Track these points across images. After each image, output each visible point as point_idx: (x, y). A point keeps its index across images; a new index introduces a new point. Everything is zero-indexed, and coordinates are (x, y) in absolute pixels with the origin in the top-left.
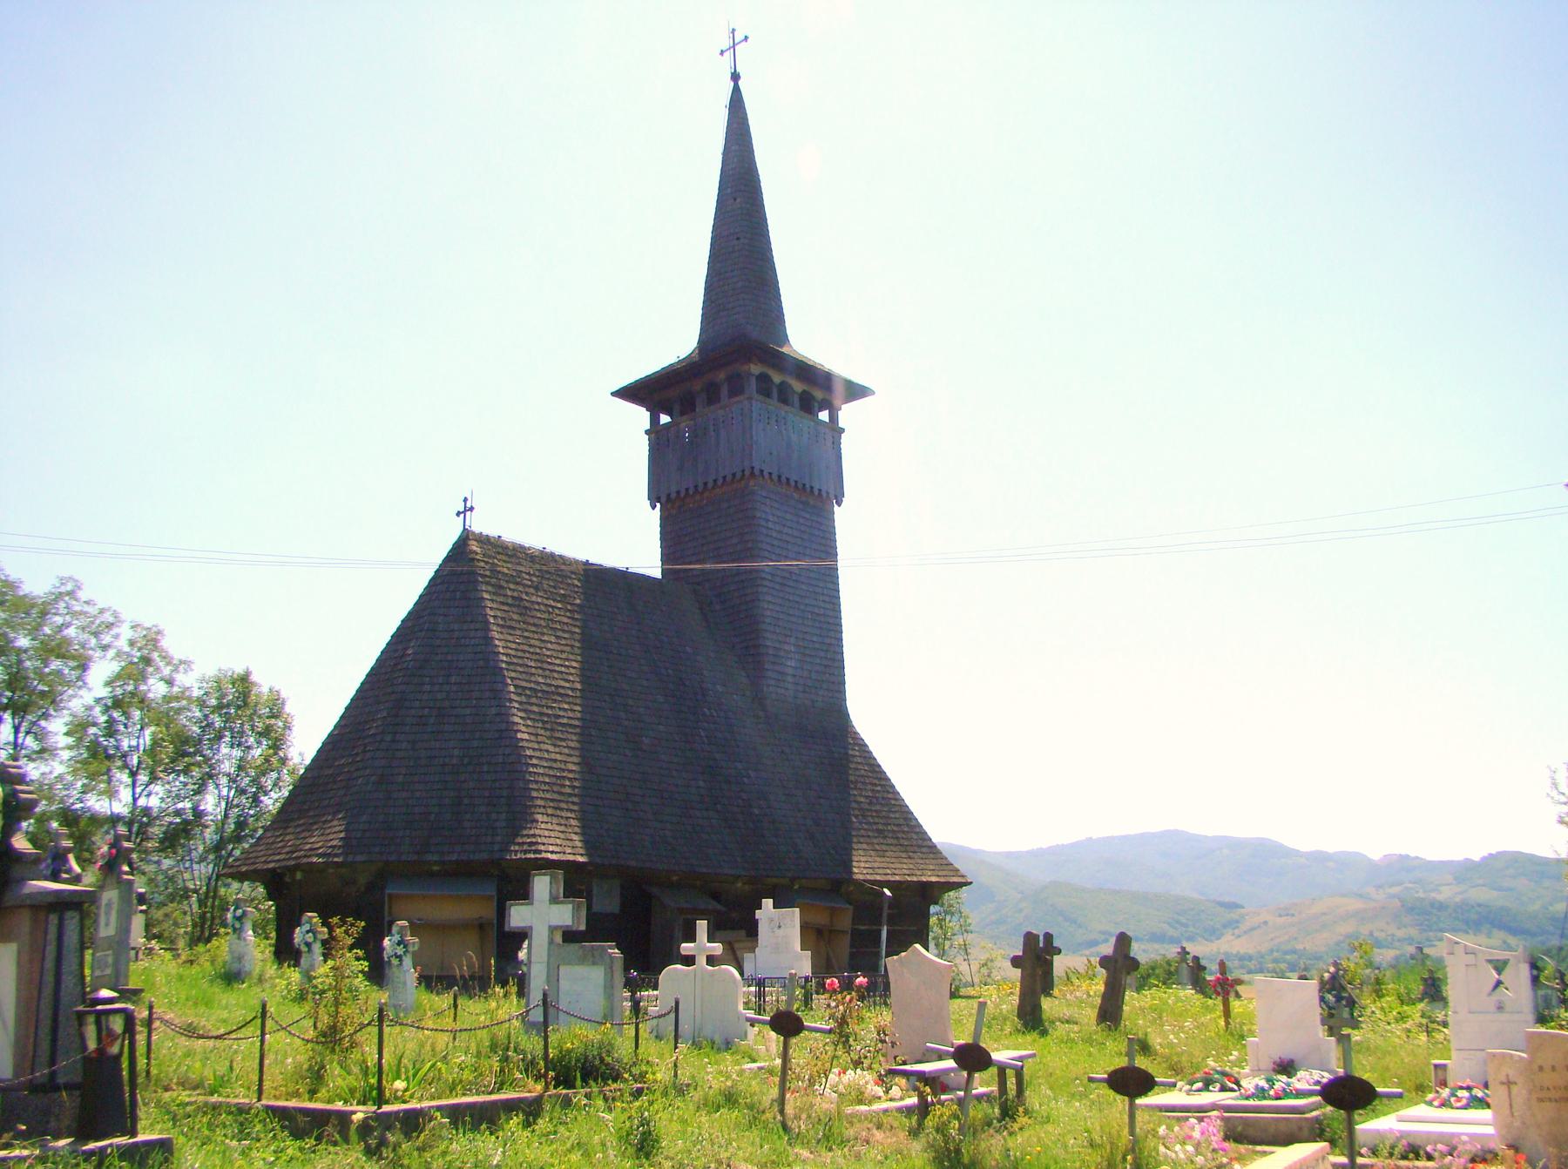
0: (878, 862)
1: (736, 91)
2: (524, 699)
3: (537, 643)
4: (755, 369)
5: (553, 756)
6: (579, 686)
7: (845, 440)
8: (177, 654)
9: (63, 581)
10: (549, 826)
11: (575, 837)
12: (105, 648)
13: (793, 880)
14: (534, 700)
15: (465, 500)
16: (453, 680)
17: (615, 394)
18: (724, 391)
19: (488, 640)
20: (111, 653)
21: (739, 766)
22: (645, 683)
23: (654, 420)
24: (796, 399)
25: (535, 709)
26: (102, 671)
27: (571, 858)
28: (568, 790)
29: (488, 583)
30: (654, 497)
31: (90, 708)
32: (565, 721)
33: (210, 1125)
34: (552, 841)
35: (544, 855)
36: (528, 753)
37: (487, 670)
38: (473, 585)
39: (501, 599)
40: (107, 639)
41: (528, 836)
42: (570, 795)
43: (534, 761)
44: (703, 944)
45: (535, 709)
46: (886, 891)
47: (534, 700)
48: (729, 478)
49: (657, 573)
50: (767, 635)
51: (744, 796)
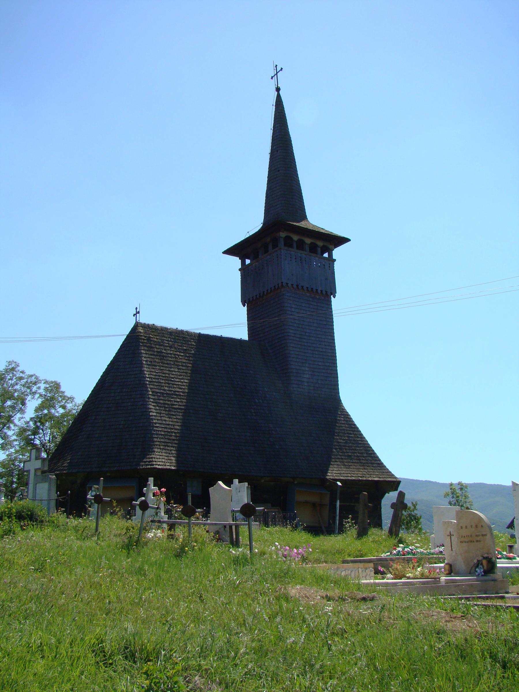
0: (344, 470)
2: (156, 397)
3: (167, 372)
4: (283, 235)
5: (167, 423)
6: (186, 391)
8: (68, 394)
9: (10, 363)
10: (160, 454)
11: (173, 458)
12: (35, 393)
14: (162, 398)
15: (136, 308)
16: (124, 390)
17: (224, 253)
18: (270, 246)
19: (142, 372)
20: (37, 396)
23: (243, 263)
24: (307, 248)
25: (162, 402)
26: (32, 405)
27: (168, 467)
28: (173, 438)
29: (145, 346)
30: (244, 303)
31: (28, 422)
32: (177, 407)
33: (92, 612)
34: (160, 460)
35: (155, 466)
36: (154, 421)
37: (140, 385)
38: (143, 346)
39: (151, 353)
40: (34, 389)
41: (149, 458)
42: (174, 440)
43: (157, 425)
44: (353, 532)
45: (162, 402)
46: (339, 483)
47: (162, 398)
48: (273, 289)
51: (271, 439)
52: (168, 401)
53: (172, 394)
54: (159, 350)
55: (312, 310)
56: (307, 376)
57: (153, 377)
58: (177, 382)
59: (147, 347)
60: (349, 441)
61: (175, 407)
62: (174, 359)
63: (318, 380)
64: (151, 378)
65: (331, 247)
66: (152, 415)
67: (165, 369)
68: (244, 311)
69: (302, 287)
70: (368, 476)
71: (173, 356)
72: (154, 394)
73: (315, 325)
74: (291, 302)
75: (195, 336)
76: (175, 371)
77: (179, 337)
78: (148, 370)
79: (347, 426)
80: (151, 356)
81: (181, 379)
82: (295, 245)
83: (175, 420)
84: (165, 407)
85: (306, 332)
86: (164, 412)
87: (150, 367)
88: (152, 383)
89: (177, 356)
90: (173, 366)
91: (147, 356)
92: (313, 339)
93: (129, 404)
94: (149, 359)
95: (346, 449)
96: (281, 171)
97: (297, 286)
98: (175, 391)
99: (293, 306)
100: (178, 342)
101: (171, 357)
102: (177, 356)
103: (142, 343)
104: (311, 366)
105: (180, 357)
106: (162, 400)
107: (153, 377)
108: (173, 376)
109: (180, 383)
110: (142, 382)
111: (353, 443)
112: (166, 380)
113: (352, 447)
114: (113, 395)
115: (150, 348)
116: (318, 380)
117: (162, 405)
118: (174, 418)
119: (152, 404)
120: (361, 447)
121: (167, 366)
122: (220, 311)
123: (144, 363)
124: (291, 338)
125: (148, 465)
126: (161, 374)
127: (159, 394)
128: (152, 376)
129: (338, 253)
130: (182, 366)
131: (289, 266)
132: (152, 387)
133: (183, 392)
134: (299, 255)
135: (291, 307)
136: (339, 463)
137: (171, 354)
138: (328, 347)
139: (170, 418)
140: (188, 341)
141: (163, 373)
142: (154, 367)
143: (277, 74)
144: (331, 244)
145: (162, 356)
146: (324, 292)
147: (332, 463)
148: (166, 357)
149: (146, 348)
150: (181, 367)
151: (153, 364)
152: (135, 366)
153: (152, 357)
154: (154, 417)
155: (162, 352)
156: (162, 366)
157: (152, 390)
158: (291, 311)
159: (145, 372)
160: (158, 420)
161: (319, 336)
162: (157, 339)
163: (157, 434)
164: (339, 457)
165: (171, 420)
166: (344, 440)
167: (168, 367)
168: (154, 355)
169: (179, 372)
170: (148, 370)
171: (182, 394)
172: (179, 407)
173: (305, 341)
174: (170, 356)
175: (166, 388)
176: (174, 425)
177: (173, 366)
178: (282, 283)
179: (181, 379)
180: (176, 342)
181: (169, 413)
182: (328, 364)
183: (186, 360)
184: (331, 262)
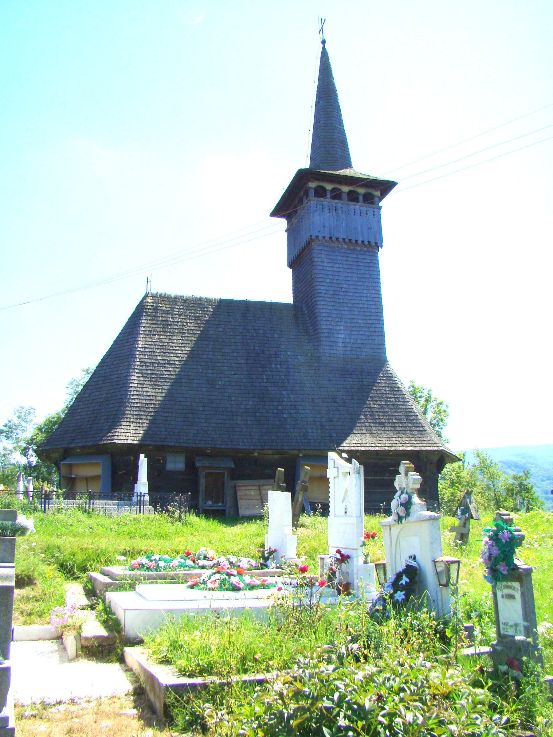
2: (144, 368)
4: (312, 185)
5: (149, 394)
10: (128, 427)
13: (299, 450)
21: (284, 392)
22: (235, 354)
25: (149, 372)
32: (167, 376)
34: (124, 434)
35: (115, 441)
36: (132, 393)
42: (151, 412)
43: (135, 397)
51: (280, 407)
52: (158, 371)
53: (165, 364)
60: (385, 406)
61: (164, 376)
62: (181, 327)
64: (145, 348)
66: (132, 387)
68: (290, 271)
69: (337, 239)
70: (400, 445)
71: (180, 323)
73: (354, 279)
74: (323, 256)
79: (387, 389)
81: (182, 347)
84: (151, 378)
85: (341, 288)
86: (148, 383)
87: (147, 337)
88: (143, 353)
89: (185, 324)
92: (351, 294)
95: (379, 415)
97: (331, 238)
103: (146, 312)
104: (349, 325)
105: (189, 324)
106: (151, 370)
108: (173, 345)
111: (391, 408)
112: (163, 349)
113: (388, 412)
120: (400, 412)
121: (169, 334)
122: (263, 274)
124: (323, 295)
125: (109, 440)
127: (148, 364)
129: (388, 205)
130: (188, 333)
131: (321, 217)
133: (179, 361)
136: (364, 432)
137: (178, 322)
138: (371, 303)
139: (153, 389)
144: (376, 191)
145: (166, 324)
146: (366, 243)
147: (355, 432)
148: (170, 325)
153: (154, 326)
159: (139, 342)
161: (360, 291)
162: (166, 307)
163: (131, 407)
164: (367, 424)
165: (154, 391)
166: (379, 405)
167: (169, 336)
168: (156, 324)
172: (170, 377)
173: (340, 297)
175: (159, 358)
176: (156, 396)
180: (189, 310)
181: (155, 383)
182: (371, 322)
184: (376, 210)
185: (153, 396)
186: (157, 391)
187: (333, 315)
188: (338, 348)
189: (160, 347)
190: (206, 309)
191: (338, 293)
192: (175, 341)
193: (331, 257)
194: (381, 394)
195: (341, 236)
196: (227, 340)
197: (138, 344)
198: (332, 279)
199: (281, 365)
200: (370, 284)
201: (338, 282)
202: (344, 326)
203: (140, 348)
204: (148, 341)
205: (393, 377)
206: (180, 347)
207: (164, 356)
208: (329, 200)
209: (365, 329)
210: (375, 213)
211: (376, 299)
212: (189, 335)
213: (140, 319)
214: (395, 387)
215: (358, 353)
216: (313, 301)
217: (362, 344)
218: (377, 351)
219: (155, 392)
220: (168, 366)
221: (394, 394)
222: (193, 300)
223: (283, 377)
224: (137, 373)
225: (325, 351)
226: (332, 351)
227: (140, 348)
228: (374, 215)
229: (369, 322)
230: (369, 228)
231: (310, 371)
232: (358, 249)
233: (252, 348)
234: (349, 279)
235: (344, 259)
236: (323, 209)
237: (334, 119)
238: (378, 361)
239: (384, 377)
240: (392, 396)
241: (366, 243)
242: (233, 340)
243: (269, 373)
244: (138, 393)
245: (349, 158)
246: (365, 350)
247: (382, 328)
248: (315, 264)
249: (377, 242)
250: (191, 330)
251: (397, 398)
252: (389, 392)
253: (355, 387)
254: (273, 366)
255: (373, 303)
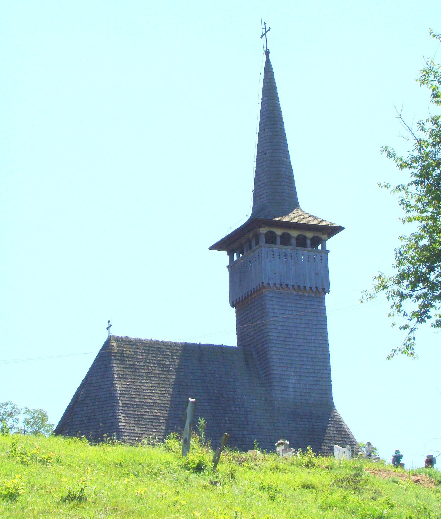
1: (268, 61)
2: (126, 409)
4: (263, 231)
5: (136, 432)
7: (329, 256)
15: (109, 322)
16: (96, 404)
19: (113, 385)
21: (245, 433)
23: (231, 259)
24: (294, 242)
25: (131, 412)
29: (118, 359)
32: (147, 417)
36: (123, 431)
37: (111, 397)
39: (123, 366)
43: (126, 434)
47: (132, 409)
49: (230, 339)
50: (275, 368)
52: (138, 411)
53: (142, 405)
54: (131, 363)
55: (299, 310)
56: (293, 381)
57: (124, 389)
58: (148, 393)
59: (120, 360)
61: (145, 417)
62: (147, 371)
63: (306, 385)
64: (122, 390)
65: (324, 237)
66: (121, 425)
67: (136, 381)
68: (233, 311)
69: (287, 285)
72: (125, 405)
75: (171, 346)
76: (147, 383)
77: (155, 348)
78: (120, 383)
79: (335, 432)
80: (123, 370)
81: (153, 390)
82: (278, 240)
83: (144, 429)
84: (134, 418)
86: (133, 422)
87: (122, 380)
88: (123, 396)
89: (150, 368)
90: (145, 378)
91: (119, 369)
93: (101, 416)
94: (120, 373)
96: (267, 155)
97: (281, 285)
98: (146, 402)
99: (276, 307)
100: (152, 354)
101: (144, 369)
102: (150, 368)
103: (114, 356)
104: (298, 370)
105: (154, 368)
106: (132, 411)
107: (124, 389)
108: (144, 388)
109: (151, 394)
110: (113, 395)
112: (137, 392)
114: (85, 408)
115: (122, 361)
116: (306, 385)
117: (132, 416)
118: (143, 428)
119: (122, 415)
121: (138, 378)
123: (116, 376)
124: (274, 341)
126: (132, 386)
127: (129, 406)
128: (123, 389)
129: (332, 243)
130: (155, 377)
131: (272, 264)
132: (122, 399)
133: (154, 403)
134: (284, 250)
135: (274, 309)
137: (144, 366)
138: (318, 349)
139: (138, 427)
140: (163, 351)
141: (135, 385)
142: (125, 380)
143: (265, 34)
144: (323, 234)
145: (134, 369)
146: (314, 289)
148: (138, 369)
149: (118, 362)
150: (154, 378)
151: (125, 376)
152: (107, 380)
153: (124, 370)
154: (122, 427)
155: (134, 365)
156: (134, 379)
157: (123, 402)
158: (274, 313)
159: (117, 385)
160: (126, 429)
161: (308, 337)
162: (130, 351)
165: (139, 429)
167: (140, 379)
168: (126, 368)
169: (151, 383)
170: (120, 383)
171: (152, 405)
172: (149, 417)
173: (290, 343)
174: (142, 367)
175: (137, 400)
177: (145, 378)
178: (263, 283)
179: (153, 390)
180: (150, 353)
181: (139, 423)
182: (319, 367)
183: (160, 371)
184: (323, 255)
185: (140, 433)
186: (142, 429)
187: (283, 361)
188: (288, 393)
189: (135, 390)
190: (164, 353)
191: (288, 339)
192: (146, 384)
193: (282, 304)
194: (330, 437)
195: (291, 283)
196: (189, 384)
197: (116, 387)
198: (283, 326)
199: (239, 408)
200: (318, 331)
201: (288, 328)
202: (294, 372)
203: (119, 390)
204: (124, 384)
205: (340, 421)
206: (151, 390)
207: (140, 398)
208: (278, 245)
209: (313, 375)
210: (323, 258)
211: (324, 345)
212: (156, 379)
213: (110, 363)
214: (342, 431)
215: (307, 398)
216: (265, 346)
217: (311, 389)
218: (325, 396)
219: (140, 430)
220: (146, 407)
221: (342, 438)
222: (151, 344)
223: (243, 419)
224: (122, 413)
225: (277, 396)
226: (283, 396)
227: (119, 390)
228: (321, 260)
229: (317, 367)
230: (317, 274)
231: (266, 414)
232: (306, 294)
233: (212, 391)
234: (298, 325)
235: (293, 305)
236: (273, 255)
237: (281, 151)
238: (329, 406)
239: (332, 421)
240: (340, 439)
241: (314, 289)
242: (194, 384)
243: (230, 415)
244: (127, 431)
245: (296, 195)
246: (314, 395)
247: (329, 374)
248: (267, 310)
249: (325, 287)
250: (156, 374)
251: (345, 441)
252: (337, 436)
253: (307, 430)
254: (233, 409)
255: (321, 349)
